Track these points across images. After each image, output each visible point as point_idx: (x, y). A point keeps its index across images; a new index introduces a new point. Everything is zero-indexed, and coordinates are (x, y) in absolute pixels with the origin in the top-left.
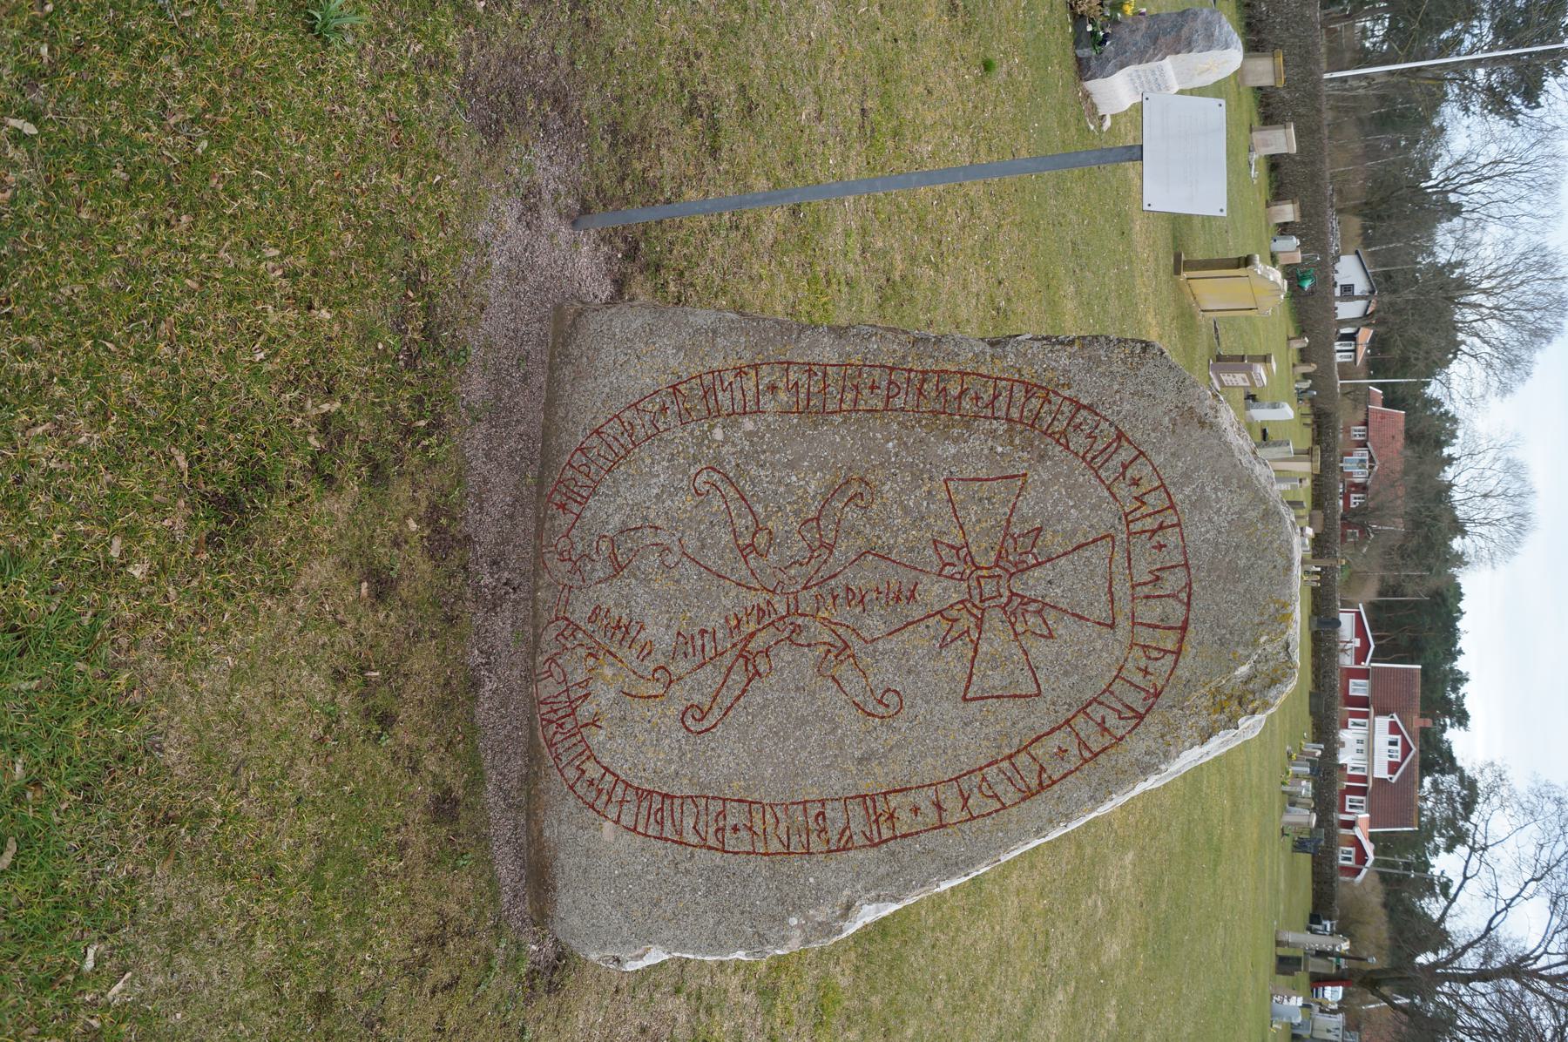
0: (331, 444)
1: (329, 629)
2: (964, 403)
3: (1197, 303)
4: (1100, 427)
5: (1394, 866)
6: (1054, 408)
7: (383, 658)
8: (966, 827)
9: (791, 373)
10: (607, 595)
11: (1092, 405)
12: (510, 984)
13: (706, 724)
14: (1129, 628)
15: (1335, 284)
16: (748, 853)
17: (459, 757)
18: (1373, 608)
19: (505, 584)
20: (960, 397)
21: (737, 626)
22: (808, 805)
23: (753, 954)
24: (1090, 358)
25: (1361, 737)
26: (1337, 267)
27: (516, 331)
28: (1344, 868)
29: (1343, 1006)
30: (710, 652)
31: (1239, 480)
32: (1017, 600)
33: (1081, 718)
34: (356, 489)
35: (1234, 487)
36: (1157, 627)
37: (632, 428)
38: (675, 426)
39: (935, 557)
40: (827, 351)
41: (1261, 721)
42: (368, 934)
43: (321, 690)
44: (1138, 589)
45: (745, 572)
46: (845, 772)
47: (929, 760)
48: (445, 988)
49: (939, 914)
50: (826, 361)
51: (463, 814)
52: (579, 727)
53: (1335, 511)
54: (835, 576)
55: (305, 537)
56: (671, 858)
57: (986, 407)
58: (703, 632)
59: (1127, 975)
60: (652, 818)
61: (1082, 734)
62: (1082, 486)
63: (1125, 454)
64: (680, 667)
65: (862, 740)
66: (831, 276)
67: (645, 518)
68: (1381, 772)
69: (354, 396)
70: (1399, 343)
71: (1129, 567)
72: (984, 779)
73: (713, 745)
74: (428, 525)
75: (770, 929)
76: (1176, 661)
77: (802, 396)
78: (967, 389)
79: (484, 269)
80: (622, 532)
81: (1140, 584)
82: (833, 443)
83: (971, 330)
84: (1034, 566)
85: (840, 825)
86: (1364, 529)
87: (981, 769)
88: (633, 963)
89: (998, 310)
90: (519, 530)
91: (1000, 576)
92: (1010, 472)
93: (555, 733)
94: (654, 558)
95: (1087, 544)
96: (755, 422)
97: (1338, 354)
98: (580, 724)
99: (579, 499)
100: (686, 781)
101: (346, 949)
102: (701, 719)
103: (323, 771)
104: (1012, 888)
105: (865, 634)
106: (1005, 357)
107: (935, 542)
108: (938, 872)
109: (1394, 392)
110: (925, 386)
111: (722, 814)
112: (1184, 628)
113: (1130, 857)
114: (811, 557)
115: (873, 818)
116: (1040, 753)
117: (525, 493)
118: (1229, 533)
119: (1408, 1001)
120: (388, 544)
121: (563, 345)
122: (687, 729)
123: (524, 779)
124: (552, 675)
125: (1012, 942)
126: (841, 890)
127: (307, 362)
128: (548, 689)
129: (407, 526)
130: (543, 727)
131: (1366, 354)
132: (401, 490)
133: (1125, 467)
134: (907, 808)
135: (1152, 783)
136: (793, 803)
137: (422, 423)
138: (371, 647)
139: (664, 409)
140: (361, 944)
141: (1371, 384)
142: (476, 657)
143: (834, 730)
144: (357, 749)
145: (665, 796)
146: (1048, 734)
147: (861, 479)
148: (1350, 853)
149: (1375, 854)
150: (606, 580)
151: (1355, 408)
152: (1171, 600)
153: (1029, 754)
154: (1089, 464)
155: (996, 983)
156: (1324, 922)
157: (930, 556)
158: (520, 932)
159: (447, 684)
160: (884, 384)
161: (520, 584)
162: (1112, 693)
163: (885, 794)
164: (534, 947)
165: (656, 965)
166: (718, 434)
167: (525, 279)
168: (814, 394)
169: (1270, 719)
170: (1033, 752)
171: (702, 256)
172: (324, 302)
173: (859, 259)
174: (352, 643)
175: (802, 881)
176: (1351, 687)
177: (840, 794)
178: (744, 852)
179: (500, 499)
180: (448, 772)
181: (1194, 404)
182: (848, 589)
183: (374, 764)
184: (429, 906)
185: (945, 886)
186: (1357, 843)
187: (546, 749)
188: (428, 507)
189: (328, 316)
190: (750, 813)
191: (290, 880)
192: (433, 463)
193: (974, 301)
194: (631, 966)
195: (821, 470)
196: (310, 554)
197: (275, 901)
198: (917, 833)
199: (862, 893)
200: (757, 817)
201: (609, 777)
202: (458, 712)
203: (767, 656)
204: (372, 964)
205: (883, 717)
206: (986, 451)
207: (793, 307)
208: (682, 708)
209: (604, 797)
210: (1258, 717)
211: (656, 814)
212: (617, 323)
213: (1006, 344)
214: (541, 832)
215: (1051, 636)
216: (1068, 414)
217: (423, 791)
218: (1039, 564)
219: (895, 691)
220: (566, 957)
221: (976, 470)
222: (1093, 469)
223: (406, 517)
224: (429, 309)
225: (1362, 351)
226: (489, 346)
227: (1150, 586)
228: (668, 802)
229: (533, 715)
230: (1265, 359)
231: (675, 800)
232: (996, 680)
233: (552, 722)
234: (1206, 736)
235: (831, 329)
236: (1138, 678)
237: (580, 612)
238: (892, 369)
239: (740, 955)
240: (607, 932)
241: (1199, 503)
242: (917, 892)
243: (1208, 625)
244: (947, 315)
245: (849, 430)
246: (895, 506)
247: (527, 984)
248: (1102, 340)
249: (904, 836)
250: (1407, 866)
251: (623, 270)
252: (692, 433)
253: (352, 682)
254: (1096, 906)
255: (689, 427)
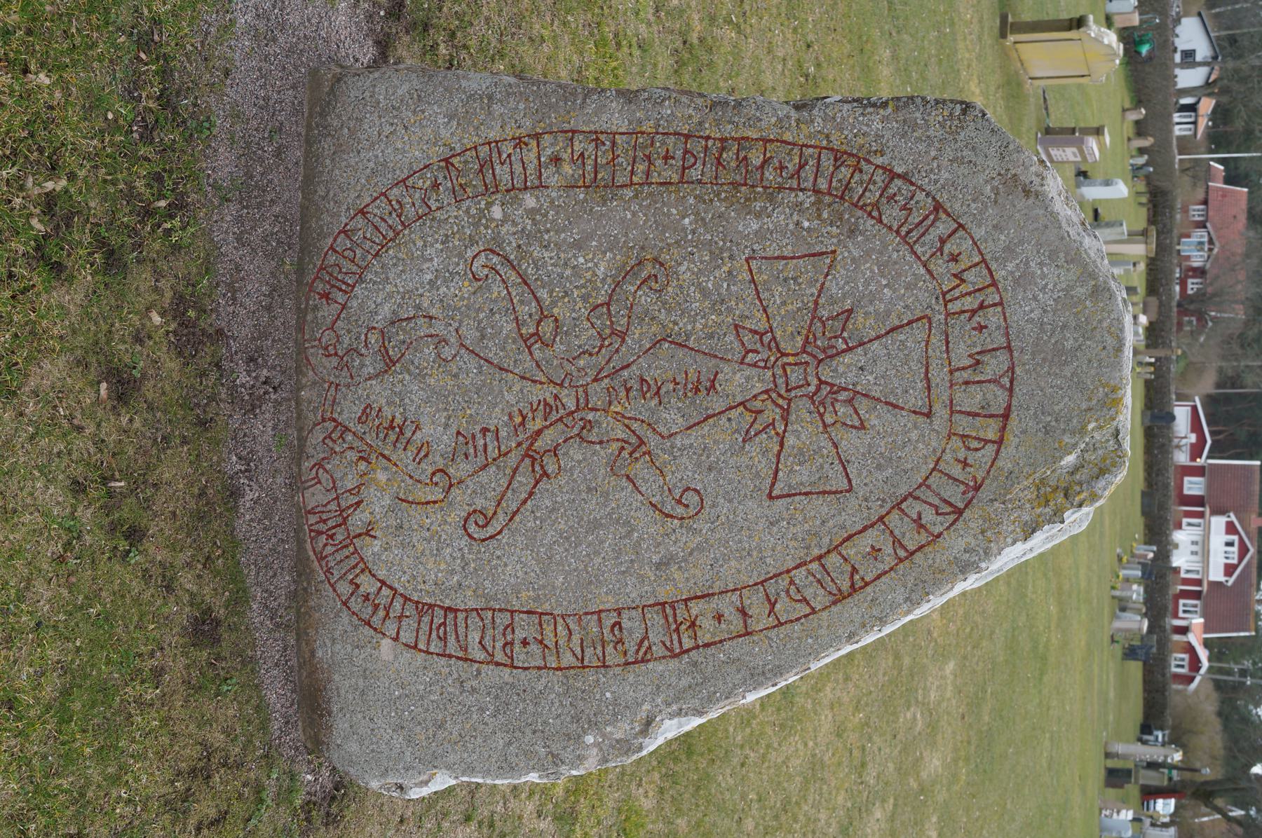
0: (57, 227)
1: (65, 435)
2: (767, 174)
3: (1025, 70)
4: (916, 199)
5: (1229, 672)
6: (866, 178)
7: (128, 466)
8: (773, 633)
9: (576, 143)
10: (378, 393)
11: (907, 173)
12: (284, 817)
13: (490, 531)
14: (947, 416)
15: (1175, 50)
16: (539, 668)
17: (219, 573)
18: (1210, 401)
19: (265, 383)
20: (762, 166)
21: (523, 424)
22: (603, 615)
23: (547, 776)
24: (905, 121)
25: (1195, 538)
26: (1178, 30)
27: (267, 99)
28: (1177, 677)
29: (1175, 820)
30: (493, 452)
31: (1067, 254)
32: (825, 390)
33: (895, 515)
34: (89, 278)
35: (1061, 262)
36: (977, 415)
37: (401, 207)
38: (449, 204)
39: (736, 344)
40: (615, 118)
41: (1088, 514)
42: (123, 769)
43: (58, 503)
44: (957, 374)
45: (529, 364)
46: (642, 579)
47: (733, 563)
48: (212, 824)
49: (748, 730)
50: (614, 128)
51: (225, 635)
52: (351, 538)
53: (1170, 297)
54: (628, 366)
55: (32, 332)
56: (455, 676)
57: (792, 177)
58: (485, 431)
59: (948, 790)
60: (434, 634)
61: (896, 532)
62: (896, 263)
63: (943, 228)
64: (460, 469)
65: (659, 544)
66: (621, 37)
67: (418, 307)
68: (1217, 574)
69: (82, 173)
70: (1243, 114)
71: (947, 351)
72: (792, 582)
73: (498, 553)
74: (174, 318)
75: (564, 748)
76: (998, 452)
77: (589, 168)
78: (771, 157)
79: (227, 27)
80: (393, 323)
81: (958, 369)
82: (623, 220)
83: (779, 96)
84: (843, 351)
85: (638, 636)
86: (1201, 317)
87: (788, 571)
88: (417, 790)
89: (807, 76)
90: (278, 323)
91: (807, 363)
92: (818, 249)
93: (326, 545)
94: (429, 351)
95: (902, 326)
96: (537, 198)
97: (1177, 127)
98: (352, 534)
99: (344, 287)
100: (470, 593)
101: (99, 786)
102: (483, 527)
103: (65, 592)
104: (826, 702)
105: (661, 429)
106: (812, 121)
107: (736, 326)
108: (744, 683)
109: (1236, 168)
110: (725, 155)
111: (510, 627)
112: (1006, 416)
113: (951, 666)
114: (601, 347)
115: (674, 626)
116: (852, 552)
117: (284, 281)
118: (1055, 311)
119: (1242, 813)
120: (129, 339)
121: (321, 115)
122: (470, 536)
123: (293, 596)
124: (319, 482)
125: (826, 758)
126: (639, 705)
127: (25, 134)
128: (315, 497)
129: (150, 319)
130: (312, 539)
131: (1207, 126)
132: (142, 279)
133: (943, 241)
134: (710, 615)
135: (971, 582)
136: (586, 614)
137: (163, 203)
138: (114, 454)
139: (436, 185)
140: (115, 780)
141: (1212, 159)
142: (233, 464)
143: (629, 534)
144: (103, 567)
145: (449, 609)
146: (860, 532)
147: (655, 260)
148: (1183, 660)
149: (1210, 660)
150: (377, 376)
151: (1195, 185)
152: (992, 386)
153: (840, 554)
154: (904, 238)
155: (810, 802)
156: (1156, 733)
157: (731, 342)
158: (293, 761)
159: (202, 493)
160: (679, 153)
161: (281, 383)
162: (929, 487)
163: (686, 600)
164: (309, 777)
165: (444, 791)
166: (497, 212)
167: (274, 40)
168: (602, 166)
169: (1099, 512)
170: (844, 553)
171: (476, 14)
172: (42, 65)
173: (653, 19)
174: (92, 450)
175: (598, 697)
176: (1186, 485)
177: (637, 602)
178: (534, 668)
179: (255, 289)
180: (207, 590)
181: (1019, 171)
182: (643, 380)
183: (122, 584)
184: (190, 736)
185: (751, 697)
186: (1190, 650)
187: (316, 563)
188: (173, 298)
189: (47, 81)
190: (541, 625)
191: (32, 713)
192: (176, 248)
193: (780, 67)
194: (415, 794)
195: (611, 250)
196: (39, 352)
197: (15, 737)
198: (721, 642)
199: (663, 707)
200: (548, 630)
201: (386, 592)
202: (215, 525)
203: (556, 455)
204: (129, 801)
205: (682, 518)
206: (791, 227)
207: (579, 72)
208: (464, 514)
209: (381, 613)
210: (1085, 510)
211: (438, 629)
212: (381, 89)
213: (813, 107)
214: (313, 653)
215: (862, 427)
216: (881, 184)
217: (179, 611)
218: (849, 349)
219: (695, 490)
220: (345, 787)
221: (780, 248)
222: (908, 244)
223: (148, 309)
224: (165, 74)
225: (1203, 123)
226: (236, 116)
227: (969, 371)
228: (451, 616)
229: (300, 527)
230: (1098, 131)
231: (459, 614)
232: (803, 475)
233: (322, 533)
234: (1029, 531)
235: (620, 93)
236: (956, 471)
237: (349, 412)
238: (687, 137)
239: (533, 777)
240: (389, 758)
241: (1023, 279)
242: (722, 704)
243: (1032, 412)
244: (750, 82)
245: (641, 205)
246: (692, 288)
247: (302, 816)
248: (919, 101)
249: (707, 645)
250: (1243, 673)
251: (387, 29)
252: (467, 211)
253: (93, 494)
254: (915, 718)
255: (465, 205)
